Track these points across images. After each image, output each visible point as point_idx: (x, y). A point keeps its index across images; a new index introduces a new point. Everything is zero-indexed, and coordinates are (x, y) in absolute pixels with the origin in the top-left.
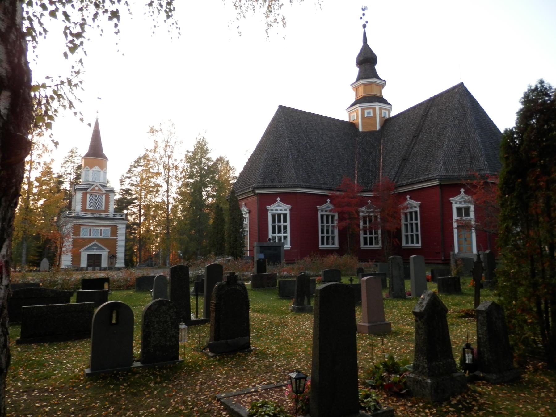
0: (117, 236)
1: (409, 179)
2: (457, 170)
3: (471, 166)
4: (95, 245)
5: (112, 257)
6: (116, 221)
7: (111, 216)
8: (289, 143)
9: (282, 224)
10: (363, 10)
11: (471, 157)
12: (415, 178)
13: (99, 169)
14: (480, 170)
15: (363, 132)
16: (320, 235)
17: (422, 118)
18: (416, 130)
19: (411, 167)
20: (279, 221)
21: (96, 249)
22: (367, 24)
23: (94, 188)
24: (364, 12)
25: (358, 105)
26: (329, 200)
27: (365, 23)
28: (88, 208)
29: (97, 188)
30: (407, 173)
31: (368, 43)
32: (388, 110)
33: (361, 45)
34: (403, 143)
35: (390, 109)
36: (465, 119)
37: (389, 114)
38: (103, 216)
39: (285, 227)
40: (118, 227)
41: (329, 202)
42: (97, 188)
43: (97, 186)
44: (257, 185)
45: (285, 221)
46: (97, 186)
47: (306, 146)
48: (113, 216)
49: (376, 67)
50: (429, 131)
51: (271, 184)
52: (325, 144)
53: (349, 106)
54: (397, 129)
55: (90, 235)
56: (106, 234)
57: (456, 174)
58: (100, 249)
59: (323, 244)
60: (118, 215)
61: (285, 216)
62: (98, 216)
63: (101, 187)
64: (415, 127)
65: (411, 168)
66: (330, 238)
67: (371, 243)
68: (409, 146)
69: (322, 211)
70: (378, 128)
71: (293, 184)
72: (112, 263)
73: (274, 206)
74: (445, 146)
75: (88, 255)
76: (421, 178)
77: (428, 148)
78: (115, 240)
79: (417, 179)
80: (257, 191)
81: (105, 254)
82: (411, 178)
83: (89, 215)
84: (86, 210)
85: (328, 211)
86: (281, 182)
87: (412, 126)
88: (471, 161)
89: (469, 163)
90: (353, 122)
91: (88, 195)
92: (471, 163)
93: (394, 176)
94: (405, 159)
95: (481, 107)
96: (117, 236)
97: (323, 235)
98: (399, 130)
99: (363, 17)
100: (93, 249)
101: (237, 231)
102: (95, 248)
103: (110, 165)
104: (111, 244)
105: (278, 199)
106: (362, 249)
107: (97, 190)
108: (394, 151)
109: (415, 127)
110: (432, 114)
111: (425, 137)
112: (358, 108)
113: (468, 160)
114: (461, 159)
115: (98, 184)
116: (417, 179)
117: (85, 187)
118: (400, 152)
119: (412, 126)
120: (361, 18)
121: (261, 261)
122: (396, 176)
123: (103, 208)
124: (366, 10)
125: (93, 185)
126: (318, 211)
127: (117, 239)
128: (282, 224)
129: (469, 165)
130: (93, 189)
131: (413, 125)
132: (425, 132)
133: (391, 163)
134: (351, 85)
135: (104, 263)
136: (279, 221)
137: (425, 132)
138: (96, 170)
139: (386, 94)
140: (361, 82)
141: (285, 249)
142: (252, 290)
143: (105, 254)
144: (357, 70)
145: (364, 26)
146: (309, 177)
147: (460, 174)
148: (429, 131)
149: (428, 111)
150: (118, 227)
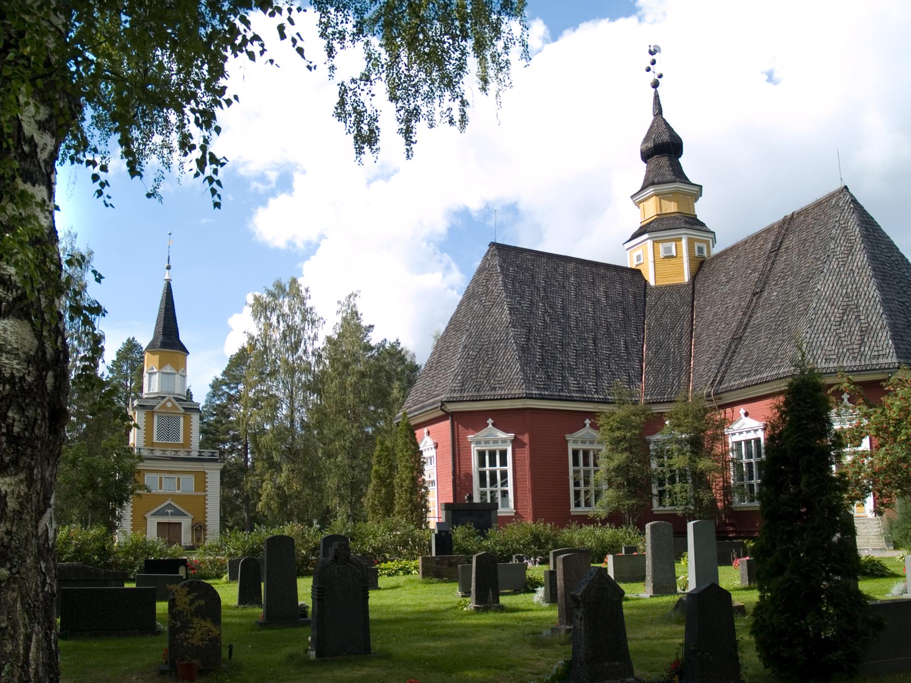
0: (207, 491)
1: (742, 377)
2: (835, 357)
3: (862, 349)
4: (169, 506)
5: (199, 528)
6: (204, 464)
7: (195, 454)
8: (510, 314)
9: (498, 468)
10: (651, 53)
11: (861, 331)
12: (755, 375)
13: (173, 371)
14: (879, 355)
15: (656, 288)
16: (572, 488)
17: (769, 257)
18: (759, 280)
19: (747, 353)
20: (492, 463)
21: (172, 514)
22: (660, 80)
23: (165, 404)
24: (654, 57)
25: (646, 236)
26: (588, 422)
27: (657, 78)
28: (155, 440)
29: (169, 405)
30: (739, 365)
31: (665, 115)
32: (707, 242)
33: (648, 118)
34: (733, 307)
35: (711, 240)
36: (850, 257)
37: (709, 252)
38: (182, 454)
39: (504, 475)
40: (207, 473)
41: (588, 425)
42: (169, 405)
43: (169, 400)
44: (448, 395)
45: (504, 463)
46: (169, 400)
47: (544, 320)
48: (197, 454)
49: (681, 160)
50: (783, 281)
51: (475, 394)
52: (580, 314)
53: (629, 238)
54: (724, 279)
55: (161, 488)
56: (188, 485)
57: (831, 365)
58: (178, 513)
59: (578, 505)
60: (207, 454)
61: (503, 454)
62: (173, 454)
63: (176, 403)
64: (756, 275)
65: (748, 355)
66: (582, 494)
67: (587, 504)
68: (744, 314)
69: (575, 442)
70: (686, 278)
71: (517, 392)
72: (198, 539)
73: (482, 434)
74: (811, 311)
75: (158, 523)
76: (765, 375)
77: (780, 317)
78: (204, 498)
79: (758, 377)
80: (451, 407)
81: (186, 523)
82: (748, 376)
83: (158, 453)
84: (153, 444)
85: (596, 443)
86: (494, 389)
87: (751, 274)
88: (863, 340)
89: (856, 342)
90: (638, 268)
91: (156, 418)
92: (862, 343)
93: (716, 371)
94: (737, 339)
95: (884, 233)
96: (207, 491)
97: (577, 488)
98: (727, 282)
99: (651, 67)
100: (167, 514)
101: (414, 480)
102: (169, 511)
103: (192, 362)
104: (198, 504)
105: (490, 421)
106: (655, 513)
107: (170, 409)
108: (717, 322)
109: (756, 275)
110: (787, 248)
111: (775, 294)
112: (646, 244)
113: (856, 338)
114: (843, 335)
115: (171, 396)
116: (758, 377)
117: (151, 403)
118: (728, 324)
119: (751, 274)
120: (648, 70)
121: (443, 534)
122: (718, 372)
123: (181, 441)
124: (657, 54)
125: (164, 398)
126: (567, 442)
127: (206, 495)
128: (498, 468)
129: (858, 346)
130: (164, 405)
131: (754, 271)
132: (775, 285)
133: (711, 347)
134: (632, 197)
135: (186, 538)
136: (492, 463)
137: (775, 285)
138: (168, 371)
139: (702, 210)
140: (650, 190)
141: (499, 515)
142: (422, 583)
143: (186, 523)
144: (641, 168)
145: (655, 85)
146: (549, 378)
147: (840, 364)
148: (783, 281)
149: (782, 242)
150: (207, 473)
